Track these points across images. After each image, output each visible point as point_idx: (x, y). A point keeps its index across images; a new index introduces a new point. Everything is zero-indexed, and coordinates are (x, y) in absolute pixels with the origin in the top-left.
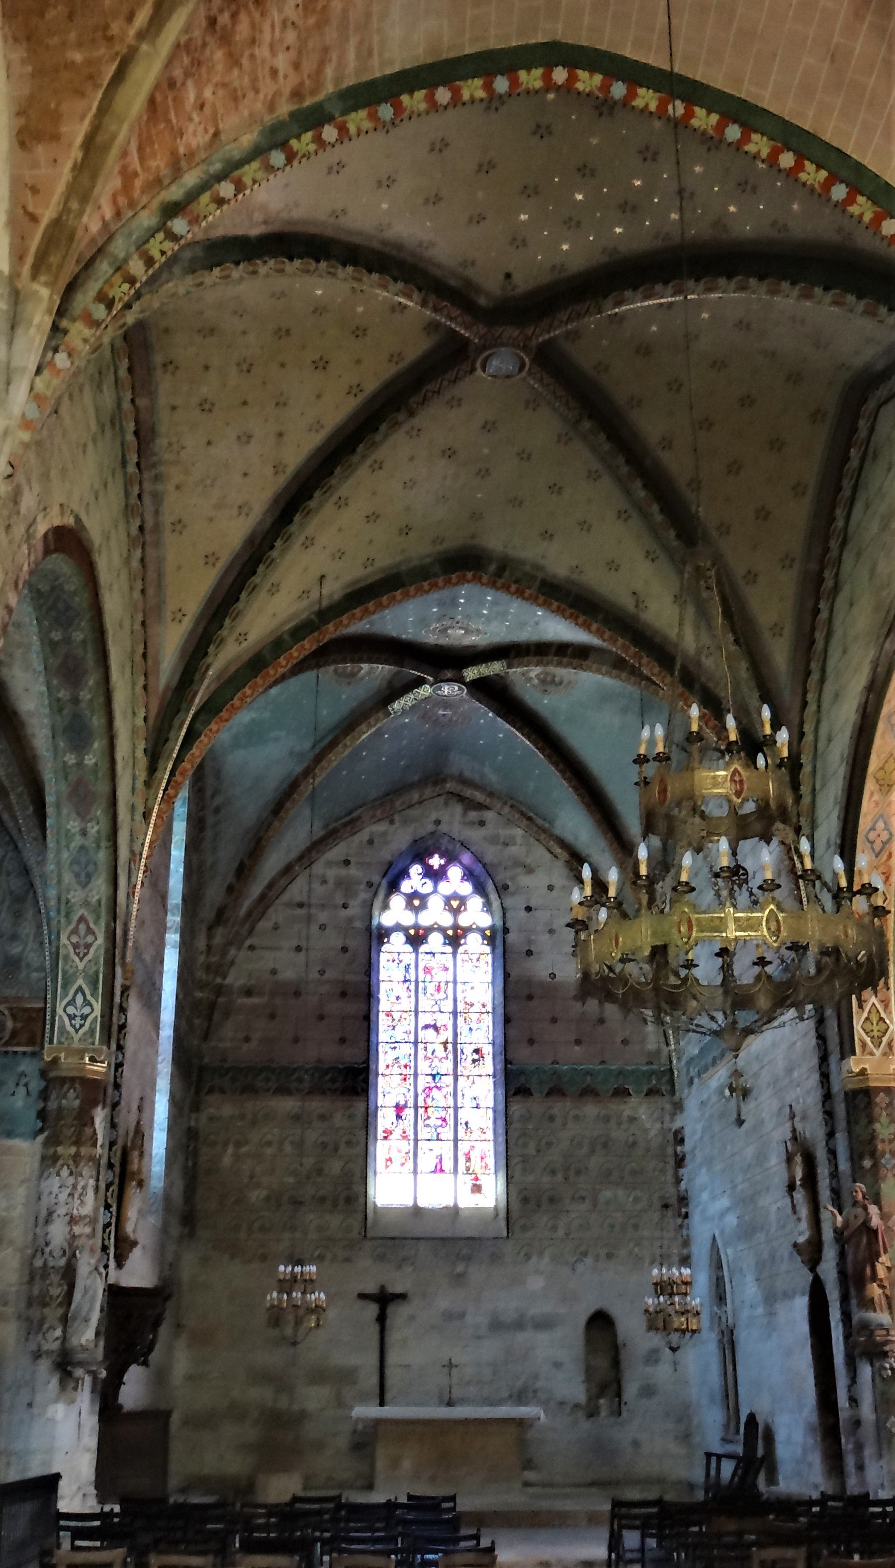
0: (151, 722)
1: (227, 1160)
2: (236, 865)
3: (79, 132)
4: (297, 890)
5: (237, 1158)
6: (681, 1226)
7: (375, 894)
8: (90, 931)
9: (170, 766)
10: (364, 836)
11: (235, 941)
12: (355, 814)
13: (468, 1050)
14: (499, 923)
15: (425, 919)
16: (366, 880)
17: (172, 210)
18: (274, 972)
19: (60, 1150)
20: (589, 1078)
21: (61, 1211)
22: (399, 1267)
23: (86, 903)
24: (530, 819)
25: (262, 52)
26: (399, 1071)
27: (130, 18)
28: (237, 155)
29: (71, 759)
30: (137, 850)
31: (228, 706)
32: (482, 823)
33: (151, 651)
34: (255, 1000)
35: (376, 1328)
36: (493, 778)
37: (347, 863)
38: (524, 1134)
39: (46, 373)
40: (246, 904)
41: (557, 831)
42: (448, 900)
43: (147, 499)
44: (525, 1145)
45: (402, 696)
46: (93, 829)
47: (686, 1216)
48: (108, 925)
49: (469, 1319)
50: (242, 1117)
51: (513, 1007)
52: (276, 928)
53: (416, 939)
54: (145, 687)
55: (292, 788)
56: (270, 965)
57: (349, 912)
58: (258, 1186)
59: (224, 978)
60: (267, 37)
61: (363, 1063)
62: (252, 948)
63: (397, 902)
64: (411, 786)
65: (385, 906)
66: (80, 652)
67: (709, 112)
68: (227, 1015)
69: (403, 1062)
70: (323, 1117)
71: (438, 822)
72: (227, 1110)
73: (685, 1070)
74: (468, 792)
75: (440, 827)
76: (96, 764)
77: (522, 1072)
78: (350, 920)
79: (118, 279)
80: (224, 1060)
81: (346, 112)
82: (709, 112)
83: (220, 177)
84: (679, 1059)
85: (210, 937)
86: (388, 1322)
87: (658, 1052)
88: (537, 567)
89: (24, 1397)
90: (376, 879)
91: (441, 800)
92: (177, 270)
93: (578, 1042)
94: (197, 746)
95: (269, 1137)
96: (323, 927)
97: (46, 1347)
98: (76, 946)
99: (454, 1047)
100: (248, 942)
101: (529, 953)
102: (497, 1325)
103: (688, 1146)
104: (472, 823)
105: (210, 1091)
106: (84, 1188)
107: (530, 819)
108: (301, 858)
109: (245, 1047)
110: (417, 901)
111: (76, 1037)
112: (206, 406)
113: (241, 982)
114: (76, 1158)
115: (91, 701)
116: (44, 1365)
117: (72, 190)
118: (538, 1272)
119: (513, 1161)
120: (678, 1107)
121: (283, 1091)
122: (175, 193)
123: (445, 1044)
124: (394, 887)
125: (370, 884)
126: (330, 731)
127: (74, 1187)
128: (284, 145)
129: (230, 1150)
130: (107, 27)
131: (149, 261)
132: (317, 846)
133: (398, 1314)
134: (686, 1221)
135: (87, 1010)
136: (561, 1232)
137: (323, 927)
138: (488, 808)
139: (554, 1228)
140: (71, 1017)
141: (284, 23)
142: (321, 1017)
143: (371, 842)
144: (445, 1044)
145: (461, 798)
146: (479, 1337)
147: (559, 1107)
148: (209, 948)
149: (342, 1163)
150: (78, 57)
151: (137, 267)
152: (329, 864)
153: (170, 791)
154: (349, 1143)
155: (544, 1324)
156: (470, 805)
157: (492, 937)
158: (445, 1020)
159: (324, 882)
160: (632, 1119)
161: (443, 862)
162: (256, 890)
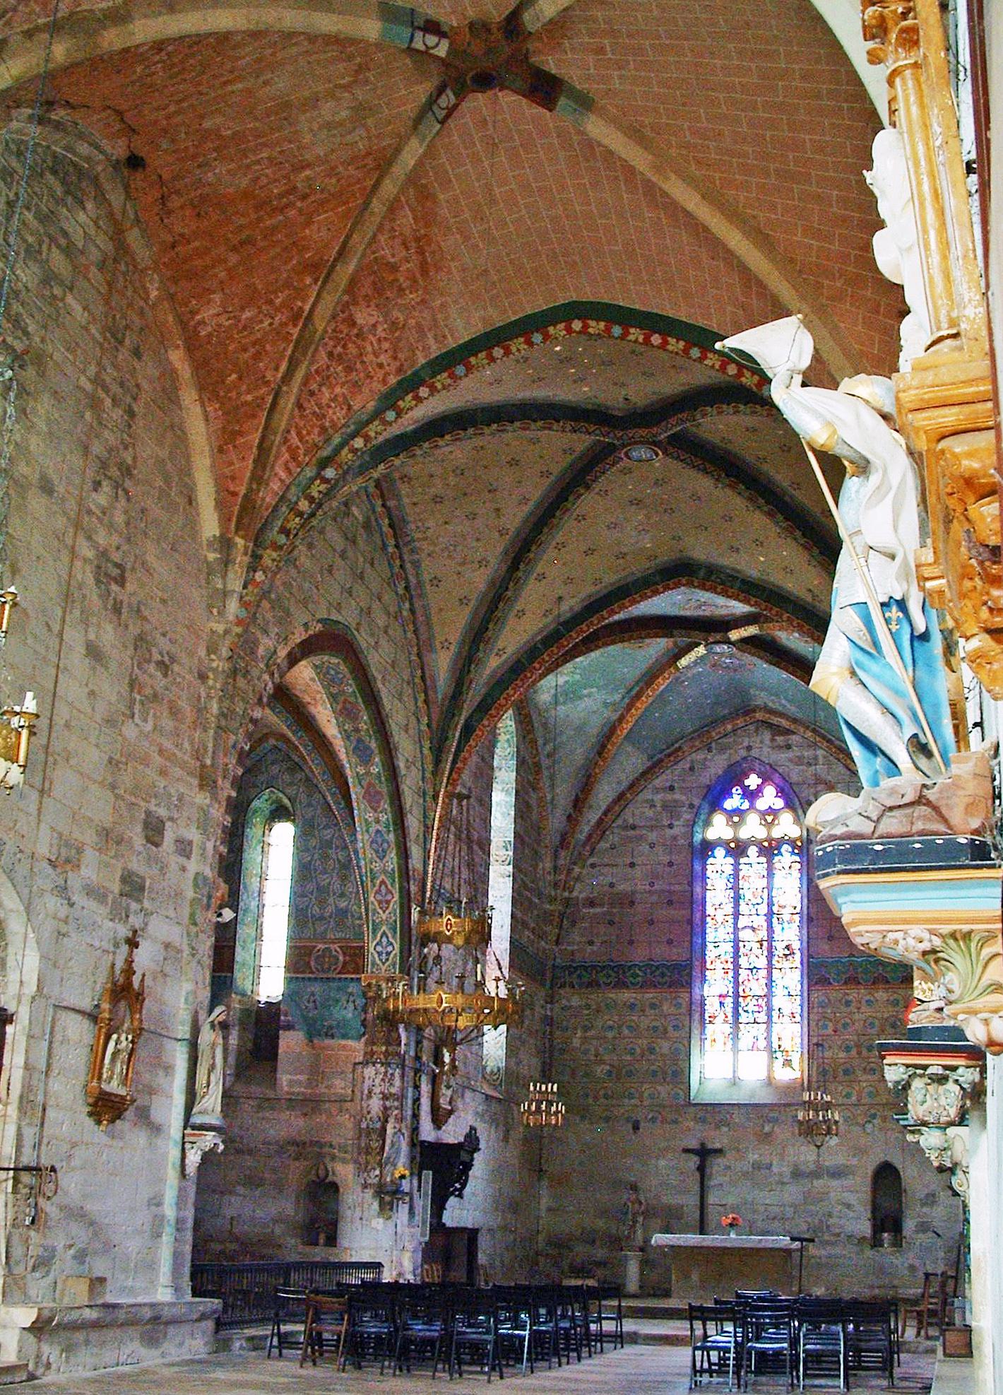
0: (434, 725)
1: (576, 1042)
3: (256, 438)
4: (632, 814)
5: (585, 1039)
7: (697, 815)
8: (389, 892)
9: (451, 758)
11: (578, 859)
15: (744, 834)
17: (324, 464)
18: (612, 885)
19: (375, 1048)
21: (377, 1090)
22: (717, 1127)
23: (385, 872)
24: (829, 741)
25: (369, 358)
27: (277, 369)
28: (364, 417)
29: (361, 770)
30: (429, 824)
32: (789, 747)
33: (427, 673)
34: (598, 910)
35: (697, 1174)
36: (792, 709)
37: (672, 788)
39: (250, 587)
42: (763, 814)
43: (408, 566)
46: (383, 817)
48: (401, 888)
49: (775, 1169)
50: (588, 1006)
52: (613, 847)
53: (737, 850)
54: (426, 702)
55: (610, 731)
56: (609, 879)
57: (675, 831)
58: (602, 1062)
59: (571, 892)
60: (369, 349)
62: (593, 866)
63: (719, 819)
64: (724, 720)
65: (708, 823)
66: (352, 699)
67: (678, 340)
68: (574, 923)
69: (723, 958)
70: (653, 1006)
71: (749, 748)
72: (575, 1001)
74: (775, 720)
78: (675, 838)
79: (292, 516)
81: (434, 375)
82: (678, 340)
83: (353, 436)
85: (556, 856)
86: (708, 1171)
89: (358, 1213)
91: (752, 728)
92: (349, 478)
95: (611, 1023)
96: (652, 846)
97: (369, 1181)
98: (380, 902)
99: (768, 944)
100: (591, 861)
102: (797, 1174)
104: (780, 747)
105: (561, 987)
106: (392, 1075)
107: (829, 741)
108: (631, 786)
109: (589, 948)
111: (383, 968)
112: (438, 500)
114: (387, 1054)
116: (369, 1193)
117: (252, 479)
121: (621, 985)
122: (326, 453)
123: (761, 942)
126: (637, 683)
127: (386, 1072)
128: (393, 406)
130: (264, 377)
131: (311, 500)
133: (717, 1166)
135: (390, 949)
138: (794, 733)
139: (848, 1096)
140: (380, 954)
141: (379, 340)
142: (651, 922)
143: (692, 769)
144: (761, 942)
145: (770, 726)
146: (783, 1183)
147: (853, 994)
148: (555, 868)
150: (249, 398)
151: (304, 505)
152: (657, 790)
153: (454, 776)
154: (676, 1027)
155: (837, 1173)
156: (777, 730)
158: (761, 921)
162: (592, 817)
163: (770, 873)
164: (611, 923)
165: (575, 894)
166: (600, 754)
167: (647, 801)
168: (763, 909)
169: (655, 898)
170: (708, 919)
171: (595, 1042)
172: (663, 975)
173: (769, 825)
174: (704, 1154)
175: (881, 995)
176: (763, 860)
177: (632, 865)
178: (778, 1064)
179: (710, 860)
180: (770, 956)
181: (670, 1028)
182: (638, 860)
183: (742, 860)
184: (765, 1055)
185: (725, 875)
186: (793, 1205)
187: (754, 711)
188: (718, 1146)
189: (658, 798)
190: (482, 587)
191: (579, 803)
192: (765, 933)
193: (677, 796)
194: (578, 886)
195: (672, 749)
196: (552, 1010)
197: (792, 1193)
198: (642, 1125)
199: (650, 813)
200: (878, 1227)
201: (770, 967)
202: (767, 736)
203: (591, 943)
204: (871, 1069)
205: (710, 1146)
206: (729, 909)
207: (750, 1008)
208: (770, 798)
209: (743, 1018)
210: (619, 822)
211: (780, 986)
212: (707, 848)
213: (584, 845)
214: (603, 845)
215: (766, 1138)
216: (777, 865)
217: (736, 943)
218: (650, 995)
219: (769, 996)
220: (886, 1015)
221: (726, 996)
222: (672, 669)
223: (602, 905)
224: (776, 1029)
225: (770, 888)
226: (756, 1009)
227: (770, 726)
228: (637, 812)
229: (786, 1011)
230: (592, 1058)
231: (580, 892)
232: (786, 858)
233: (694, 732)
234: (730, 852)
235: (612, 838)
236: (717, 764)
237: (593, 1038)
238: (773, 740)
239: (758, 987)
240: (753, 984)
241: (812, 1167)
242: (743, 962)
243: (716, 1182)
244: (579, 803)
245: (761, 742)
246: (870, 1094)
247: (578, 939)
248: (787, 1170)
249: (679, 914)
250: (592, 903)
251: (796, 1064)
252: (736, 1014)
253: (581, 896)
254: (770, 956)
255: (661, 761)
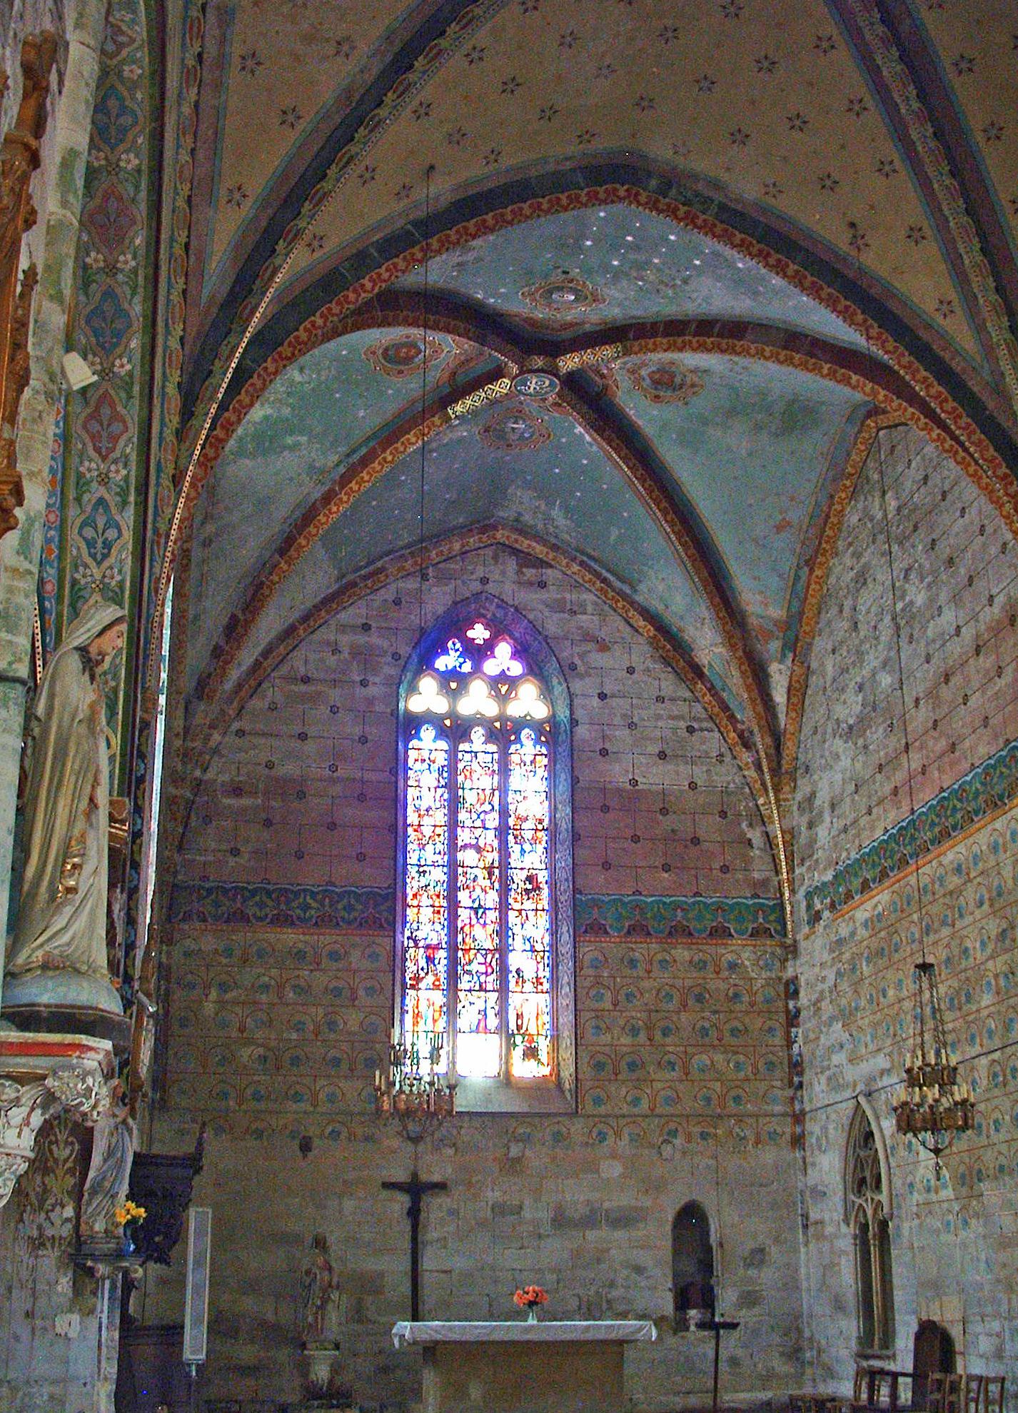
1: (209, 1008)
2: (225, 621)
4: (304, 659)
5: (221, 1003)
6: (792, 1099)
10: (388, 594)
12: (379, 564)
13: (519, 876)
14: (563, 714)
16: (392, 650)
20: (679, 913)
22: (437, 1149)
26: (430, 902)
31: (291, 338)
32: (542, 585)
34: (245, 801)
37: (366, 627)
38: (598, 983)
40: (234, 674)
41: (639, 598)
44: (600, 997)
45: (469, 394)
46: (118, 474)
47: (801, 1085)
49: (527, 1214)
50: (228, 952)
51: (584, 821)
52: (273, 708)
55: (308, 516)
56: (264, 757)
57: (372, 691)
58: (249, 1042)
61: (389, 887)
62: (241, 733)
63: (428, 684)
65: (413, 689)
68: (207, 820)
70: (334, 956)
71: (484, 581)
72: (208, 943)
73: (804, 905)
74: (524, 544)
75: (487, 587)
76: (130, 374)
77: (596, 904)
78: (370, 701)
80: (205, 878)
84: (793, 892)
87: (764, 883)
88: (716, 185)
90: (404, 650)
91: (489, 552)
93: (665, 867)
94: (247, 391)
99: (501, 873)
100: (236, 726)
101: (604, 753)
102: (560, 1221)
103: (804, 999)
105: (187, 917)
108: (305, 618)
109: (232, 861)
110: (454, 682)
113: (225, 778)
115: (135, 271)
116: (49, 1259)
118: (614, 1156)
119: (585, 1016)
120: (792, 950)
121: (282, 920)
124: (426, 663)
125: (396, 657)
129: (214, 995)
132: (330, 602)
133: (435, 1207)
134: (799, 1093)
136: (645, 1105)
137: (334, 710)
139: (636, 1102)
142: (332, 826)
143: (397, 602)
145: (515, 552)
147: (642, 950)
149: (362, 1016)
152: (343, 628)
155: (622, 1220)
156: (526, 560)
157: (549, 733)
158: (490, 838)
159: (336, 651)
160: (733, 966)
161: (487, 634)
162: (247, 656)
163: (504, 770)
164: (268, 823)
165: (210, 775)
166: (282, 552)
167: (328, 643)
168: (493, 820)
169: (337, 790)
170: (410, 830)
171: (238, 1009)
172: (349, 908)
173: (503, 699)
174: (416, 1190)
175: (682, 953)
176: (492, 748)
177: (303, 737)
178: (517, 1053)
179: (414, 743)
180: (504, 891)
181: (361, 993)
182: (312, 732)
183: (462, 747)
184: (495, 1042)
185: (434, 767)
186: (557, 1270)
187: (495, 528)
188: (436, 1178)
189: (345, 640)
190: (327, 95)
191: (235, 629)
192: (496, 855)
193: (375, 640)
194: (216, 764)
195: (371, 568)
196: (168, 953)
197: (556, 1249)
198: (317, 1142)
199: (332, 660)
200: (683, 1300)
201: (504, 907)
202: (511, 565)
203: (235, 852)
204: (670, 1063)
205: (424, 1177)
206: (440, 817)
207: (474, 967)
208: (503, 659)
209: (464, 984)
210: (284, 670)
211: (518, 939)
212: (411, 725)
213: (230, 701)
214: (257, 704)
215: (513, 1166)
216: (515, 758)
217: (453, 867)
218: (327, 939)
219: (502, 950)
220: (688, 983)
221: (437, 947)
222: (436, 420)
223: (254, 794)
224: (515, 1000)
225: (503, 789)
226: (482, 969)
227: (515, 552)
228: (312, 656)
229: (529, 974)
230: (234, 1034)
231: (218, 774)
232: (527, 748)
233: (408, 546)
234: (442, 733)
235: (272, 692)
236: (438, 600)
237: (235, 1002)
238: (519, 572)
239: (483, 936)
240: (478, 932)
241: (583, 1210)
242: (463, 896)
243: (435, 1235)
244: (235, 629)
245: (503, 573)
246: (670, 1101)
247: (213, 845)
248: (545, 1215)
249: (372, 815)
250: (237, 791)
251: (543, 1056)
252: (453, 977)
253: (221, 778)
254: (504, 891)
255: (353, 584)
